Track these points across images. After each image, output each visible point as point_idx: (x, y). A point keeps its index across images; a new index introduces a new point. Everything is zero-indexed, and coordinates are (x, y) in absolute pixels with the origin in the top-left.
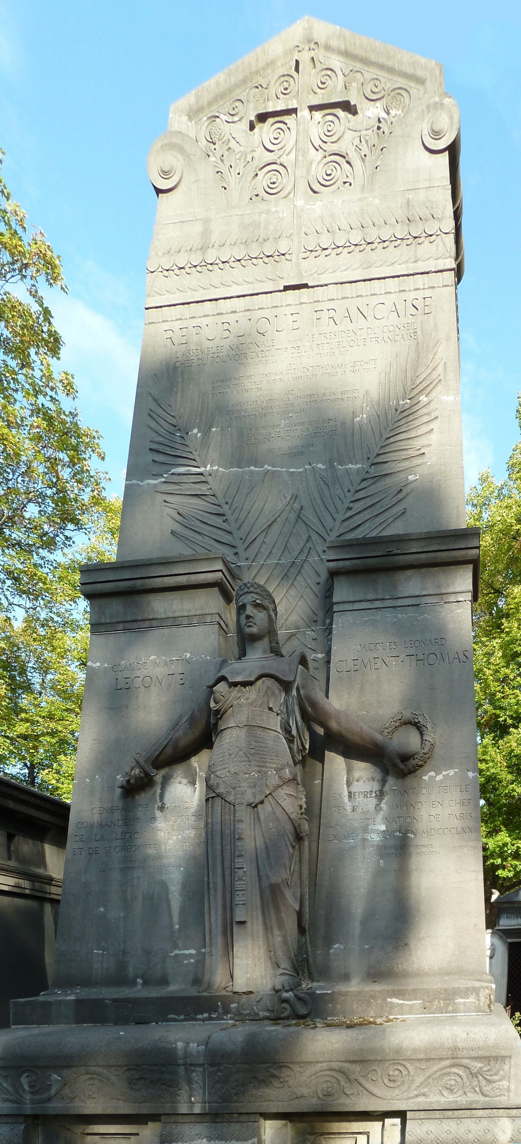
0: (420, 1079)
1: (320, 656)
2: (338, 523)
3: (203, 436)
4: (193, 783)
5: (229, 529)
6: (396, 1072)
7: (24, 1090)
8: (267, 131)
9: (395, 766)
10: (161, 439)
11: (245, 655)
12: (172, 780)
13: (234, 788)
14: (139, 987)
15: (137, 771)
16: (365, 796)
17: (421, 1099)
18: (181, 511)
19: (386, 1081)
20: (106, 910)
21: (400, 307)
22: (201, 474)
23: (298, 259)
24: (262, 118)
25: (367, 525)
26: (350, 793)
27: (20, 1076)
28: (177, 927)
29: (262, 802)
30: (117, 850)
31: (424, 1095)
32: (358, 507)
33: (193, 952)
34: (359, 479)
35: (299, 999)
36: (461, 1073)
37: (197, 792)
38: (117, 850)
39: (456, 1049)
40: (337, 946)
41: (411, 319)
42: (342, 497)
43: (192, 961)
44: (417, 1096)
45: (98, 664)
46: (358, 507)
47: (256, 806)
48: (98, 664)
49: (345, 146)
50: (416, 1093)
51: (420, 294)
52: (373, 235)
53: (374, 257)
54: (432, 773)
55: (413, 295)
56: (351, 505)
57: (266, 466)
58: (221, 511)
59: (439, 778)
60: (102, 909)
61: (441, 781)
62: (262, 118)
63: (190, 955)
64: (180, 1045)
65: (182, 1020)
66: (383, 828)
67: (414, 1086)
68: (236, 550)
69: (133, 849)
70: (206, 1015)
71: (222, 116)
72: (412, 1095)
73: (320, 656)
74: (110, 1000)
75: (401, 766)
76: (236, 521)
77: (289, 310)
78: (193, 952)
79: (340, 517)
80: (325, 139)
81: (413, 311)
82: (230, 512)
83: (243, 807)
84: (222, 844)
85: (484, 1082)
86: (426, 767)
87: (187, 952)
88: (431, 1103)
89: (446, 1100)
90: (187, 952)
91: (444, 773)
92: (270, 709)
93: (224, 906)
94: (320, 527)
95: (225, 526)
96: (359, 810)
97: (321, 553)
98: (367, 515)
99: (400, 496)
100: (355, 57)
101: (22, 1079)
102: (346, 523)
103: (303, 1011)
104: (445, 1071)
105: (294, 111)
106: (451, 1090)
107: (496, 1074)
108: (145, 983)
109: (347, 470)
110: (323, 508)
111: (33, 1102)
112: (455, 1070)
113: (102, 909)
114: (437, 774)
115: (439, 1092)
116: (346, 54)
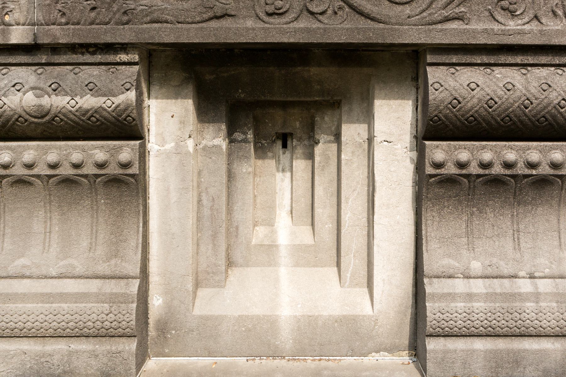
17: (454, 25)
44: (447, 19)
50: (445, 13)
72: (437, 17)
88: (474, 31)
89: (503, 27)
115: (487, 14)
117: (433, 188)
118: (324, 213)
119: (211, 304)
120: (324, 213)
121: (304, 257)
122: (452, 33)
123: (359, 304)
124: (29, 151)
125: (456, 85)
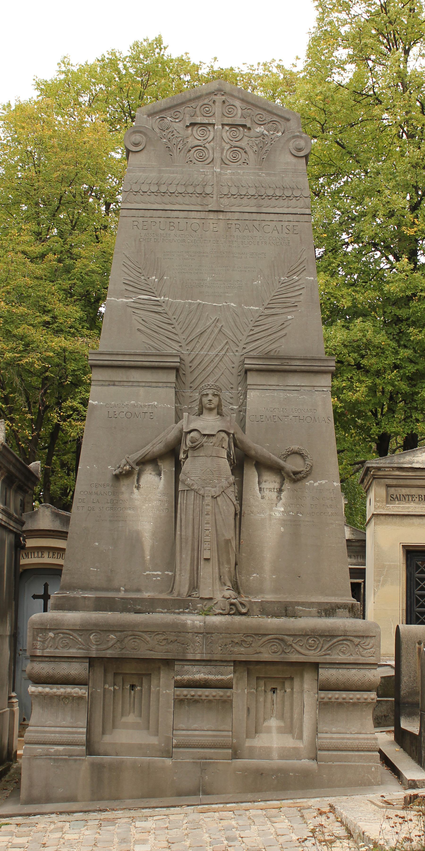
0: (325, 647)
1: (235, 407)
2: (245, 337)
3: (159, 281)
4: (159, 474)
5: (176, 332)
6: (313, 642)
7: (92, 643)
8: (197, 131)
9: (289, 476)
10: (131, 279)
11: (202, 414)
12: (145, 472)
13: (203, 487)
14: (123, 592)
15: (128, 467)
16: (270, 491)
18: (144, 319)
19: (308, 646)
20: (99, 544)
21: (279, 229)
22: (158, 301)
23: (217, 198)
24: (193, 124)
25: (263, 340)
26: (260, 488)
27: (90, 635)
28: (148, 557)
29: (219, 496)
30: (108, 509)
31: (329, 654)
32: (257, 330)
33: (159, 573)
34: (257, 315)
35: (241, 604)
36: (349, 644)
37: (162, 480)
38: (108, 509)
39: (346, 631)
40: (255, 575)
41: (286, 236)
42: (248, 324)
43: (159, 578)
44: (325, 655)
45: (96, 402)
46: (257, 330)
47: (216, 498)
48: (96, 402)
49: (243, 144)
51: (291, 224)
52: (262, 192)
53: (262, 202)
54: (312, 482)
55: (287, 223)
56: (253, 328)
57: (198, 301)
58: (171, 322)
59: (316, 484)
60: (97, 544)
61: (317, 486)
62: (193, 124)
63: (158, 575)
64: (189, 622)
65: (165, 613)
66: (282, 509)
67: (323, 650)
68: (180, 344)
69: (119, 509)
70: (181, 610)
71: (168, 118)
72: (322, 654)
73: (235, 407)
74: (118, 598)
75: (293, 477)
76: (181, 329)
77: (211, 221)
78: (159, 573)
79: (246, 334)
80: (232, 139)
81: (288, 231)
82: (177, 324)
83: (210, 498)
84: (193, 516)
85: (361, 650)
86: (308, 478)
87: (155, 573)
88: (333, 659)
90: (155, 573)
91: (319, 482)
92: (223, 448)
93: (193, 550)
94: (235, 338)
95: (173, 330)
96: (267, 498)
97: (234, 351)
98: (263, 334)
99: (283, 326)
100: (248, 103)
101: (91, 637)
102: (250, 338)
103: (244, 611)
104: (340, 642)
105: (214, 125)
106: (343, 653)
107: (368, 645)
108: (126, 591)
109: (250, 310)
110: (235, 328)
111: (97, 650)
112: (345, 642)
113: (97, 544)
114: (315, 482)
116: (242, 100)
117: (324, 706)
118: (287, 715)
119: (248, 743)
120: (287, 715)
121: (281, 731)
122: (328, 659)
123: (300, 745)
124: (213, 692)
125: (326, 674)
